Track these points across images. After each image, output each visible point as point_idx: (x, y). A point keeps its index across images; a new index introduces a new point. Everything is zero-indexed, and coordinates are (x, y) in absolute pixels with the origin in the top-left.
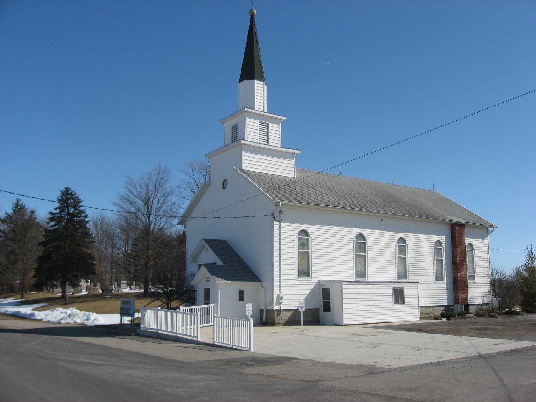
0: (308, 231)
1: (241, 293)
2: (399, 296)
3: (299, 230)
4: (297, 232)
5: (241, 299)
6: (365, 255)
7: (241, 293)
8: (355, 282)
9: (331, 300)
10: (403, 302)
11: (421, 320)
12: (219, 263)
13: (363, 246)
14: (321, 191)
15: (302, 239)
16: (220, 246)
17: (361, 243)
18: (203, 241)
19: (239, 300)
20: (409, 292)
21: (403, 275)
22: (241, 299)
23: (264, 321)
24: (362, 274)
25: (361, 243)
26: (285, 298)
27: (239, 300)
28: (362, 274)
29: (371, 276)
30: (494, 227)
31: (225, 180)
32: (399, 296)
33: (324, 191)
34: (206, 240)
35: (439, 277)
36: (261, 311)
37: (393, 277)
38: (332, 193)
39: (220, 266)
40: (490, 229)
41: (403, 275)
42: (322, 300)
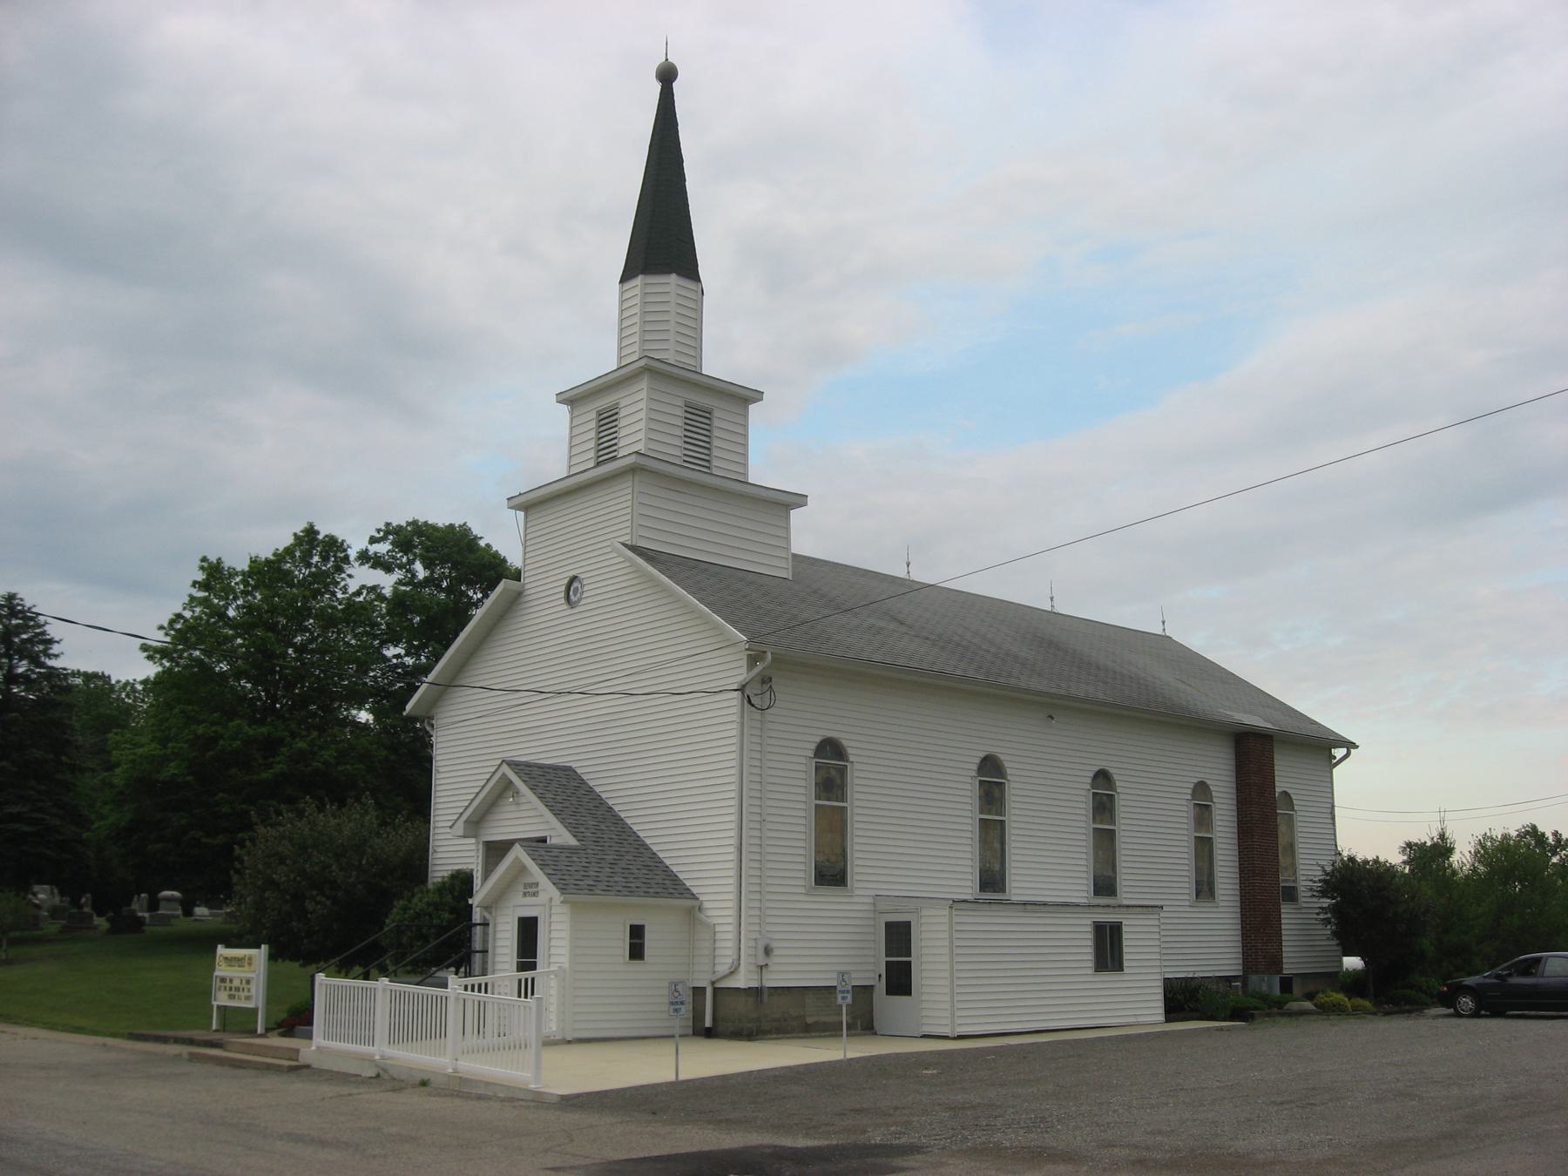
0: (845, 743)
1: (637, 932)
2: (1108, 949)
3: (818, 740)
4: (813, 746)
5: (637, 952)
6: (1002, 822)
7: (637, 932)
8: (976, 902)
9: (913, 959)
10: (1118, 967)
11: (1168, 1020)
12: (561, 836)
13: (997, 792)
14: (871, 621)
15: (828, 767)
16: (562, 787)
17: (991, 781)
18: (505, 769)
19: (907, 926)
20: (1137, 940)
21: (1105, 886)
22: (637, 952)
23: (708, 1023)
24: (992, 881)
25: (991, 781)
26: (776, 952)
27: (907, 926)
28: (992, 881)
29: (1019, 885)
30: (1350, 745)
31: (574, 579)
32: (1108, 949)
33: (882, 624)
34: (514, 765)
35: (1205, 889)
36: (698, 992)
37: (1079, 889)
38: (903, 629)
39: (562, 848)
40: (1339, 753)
41: (1105, 886)
42: (883, 959)
